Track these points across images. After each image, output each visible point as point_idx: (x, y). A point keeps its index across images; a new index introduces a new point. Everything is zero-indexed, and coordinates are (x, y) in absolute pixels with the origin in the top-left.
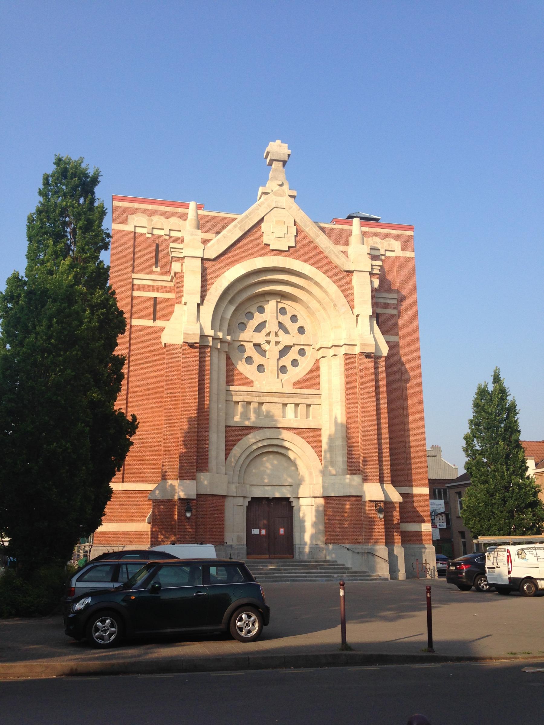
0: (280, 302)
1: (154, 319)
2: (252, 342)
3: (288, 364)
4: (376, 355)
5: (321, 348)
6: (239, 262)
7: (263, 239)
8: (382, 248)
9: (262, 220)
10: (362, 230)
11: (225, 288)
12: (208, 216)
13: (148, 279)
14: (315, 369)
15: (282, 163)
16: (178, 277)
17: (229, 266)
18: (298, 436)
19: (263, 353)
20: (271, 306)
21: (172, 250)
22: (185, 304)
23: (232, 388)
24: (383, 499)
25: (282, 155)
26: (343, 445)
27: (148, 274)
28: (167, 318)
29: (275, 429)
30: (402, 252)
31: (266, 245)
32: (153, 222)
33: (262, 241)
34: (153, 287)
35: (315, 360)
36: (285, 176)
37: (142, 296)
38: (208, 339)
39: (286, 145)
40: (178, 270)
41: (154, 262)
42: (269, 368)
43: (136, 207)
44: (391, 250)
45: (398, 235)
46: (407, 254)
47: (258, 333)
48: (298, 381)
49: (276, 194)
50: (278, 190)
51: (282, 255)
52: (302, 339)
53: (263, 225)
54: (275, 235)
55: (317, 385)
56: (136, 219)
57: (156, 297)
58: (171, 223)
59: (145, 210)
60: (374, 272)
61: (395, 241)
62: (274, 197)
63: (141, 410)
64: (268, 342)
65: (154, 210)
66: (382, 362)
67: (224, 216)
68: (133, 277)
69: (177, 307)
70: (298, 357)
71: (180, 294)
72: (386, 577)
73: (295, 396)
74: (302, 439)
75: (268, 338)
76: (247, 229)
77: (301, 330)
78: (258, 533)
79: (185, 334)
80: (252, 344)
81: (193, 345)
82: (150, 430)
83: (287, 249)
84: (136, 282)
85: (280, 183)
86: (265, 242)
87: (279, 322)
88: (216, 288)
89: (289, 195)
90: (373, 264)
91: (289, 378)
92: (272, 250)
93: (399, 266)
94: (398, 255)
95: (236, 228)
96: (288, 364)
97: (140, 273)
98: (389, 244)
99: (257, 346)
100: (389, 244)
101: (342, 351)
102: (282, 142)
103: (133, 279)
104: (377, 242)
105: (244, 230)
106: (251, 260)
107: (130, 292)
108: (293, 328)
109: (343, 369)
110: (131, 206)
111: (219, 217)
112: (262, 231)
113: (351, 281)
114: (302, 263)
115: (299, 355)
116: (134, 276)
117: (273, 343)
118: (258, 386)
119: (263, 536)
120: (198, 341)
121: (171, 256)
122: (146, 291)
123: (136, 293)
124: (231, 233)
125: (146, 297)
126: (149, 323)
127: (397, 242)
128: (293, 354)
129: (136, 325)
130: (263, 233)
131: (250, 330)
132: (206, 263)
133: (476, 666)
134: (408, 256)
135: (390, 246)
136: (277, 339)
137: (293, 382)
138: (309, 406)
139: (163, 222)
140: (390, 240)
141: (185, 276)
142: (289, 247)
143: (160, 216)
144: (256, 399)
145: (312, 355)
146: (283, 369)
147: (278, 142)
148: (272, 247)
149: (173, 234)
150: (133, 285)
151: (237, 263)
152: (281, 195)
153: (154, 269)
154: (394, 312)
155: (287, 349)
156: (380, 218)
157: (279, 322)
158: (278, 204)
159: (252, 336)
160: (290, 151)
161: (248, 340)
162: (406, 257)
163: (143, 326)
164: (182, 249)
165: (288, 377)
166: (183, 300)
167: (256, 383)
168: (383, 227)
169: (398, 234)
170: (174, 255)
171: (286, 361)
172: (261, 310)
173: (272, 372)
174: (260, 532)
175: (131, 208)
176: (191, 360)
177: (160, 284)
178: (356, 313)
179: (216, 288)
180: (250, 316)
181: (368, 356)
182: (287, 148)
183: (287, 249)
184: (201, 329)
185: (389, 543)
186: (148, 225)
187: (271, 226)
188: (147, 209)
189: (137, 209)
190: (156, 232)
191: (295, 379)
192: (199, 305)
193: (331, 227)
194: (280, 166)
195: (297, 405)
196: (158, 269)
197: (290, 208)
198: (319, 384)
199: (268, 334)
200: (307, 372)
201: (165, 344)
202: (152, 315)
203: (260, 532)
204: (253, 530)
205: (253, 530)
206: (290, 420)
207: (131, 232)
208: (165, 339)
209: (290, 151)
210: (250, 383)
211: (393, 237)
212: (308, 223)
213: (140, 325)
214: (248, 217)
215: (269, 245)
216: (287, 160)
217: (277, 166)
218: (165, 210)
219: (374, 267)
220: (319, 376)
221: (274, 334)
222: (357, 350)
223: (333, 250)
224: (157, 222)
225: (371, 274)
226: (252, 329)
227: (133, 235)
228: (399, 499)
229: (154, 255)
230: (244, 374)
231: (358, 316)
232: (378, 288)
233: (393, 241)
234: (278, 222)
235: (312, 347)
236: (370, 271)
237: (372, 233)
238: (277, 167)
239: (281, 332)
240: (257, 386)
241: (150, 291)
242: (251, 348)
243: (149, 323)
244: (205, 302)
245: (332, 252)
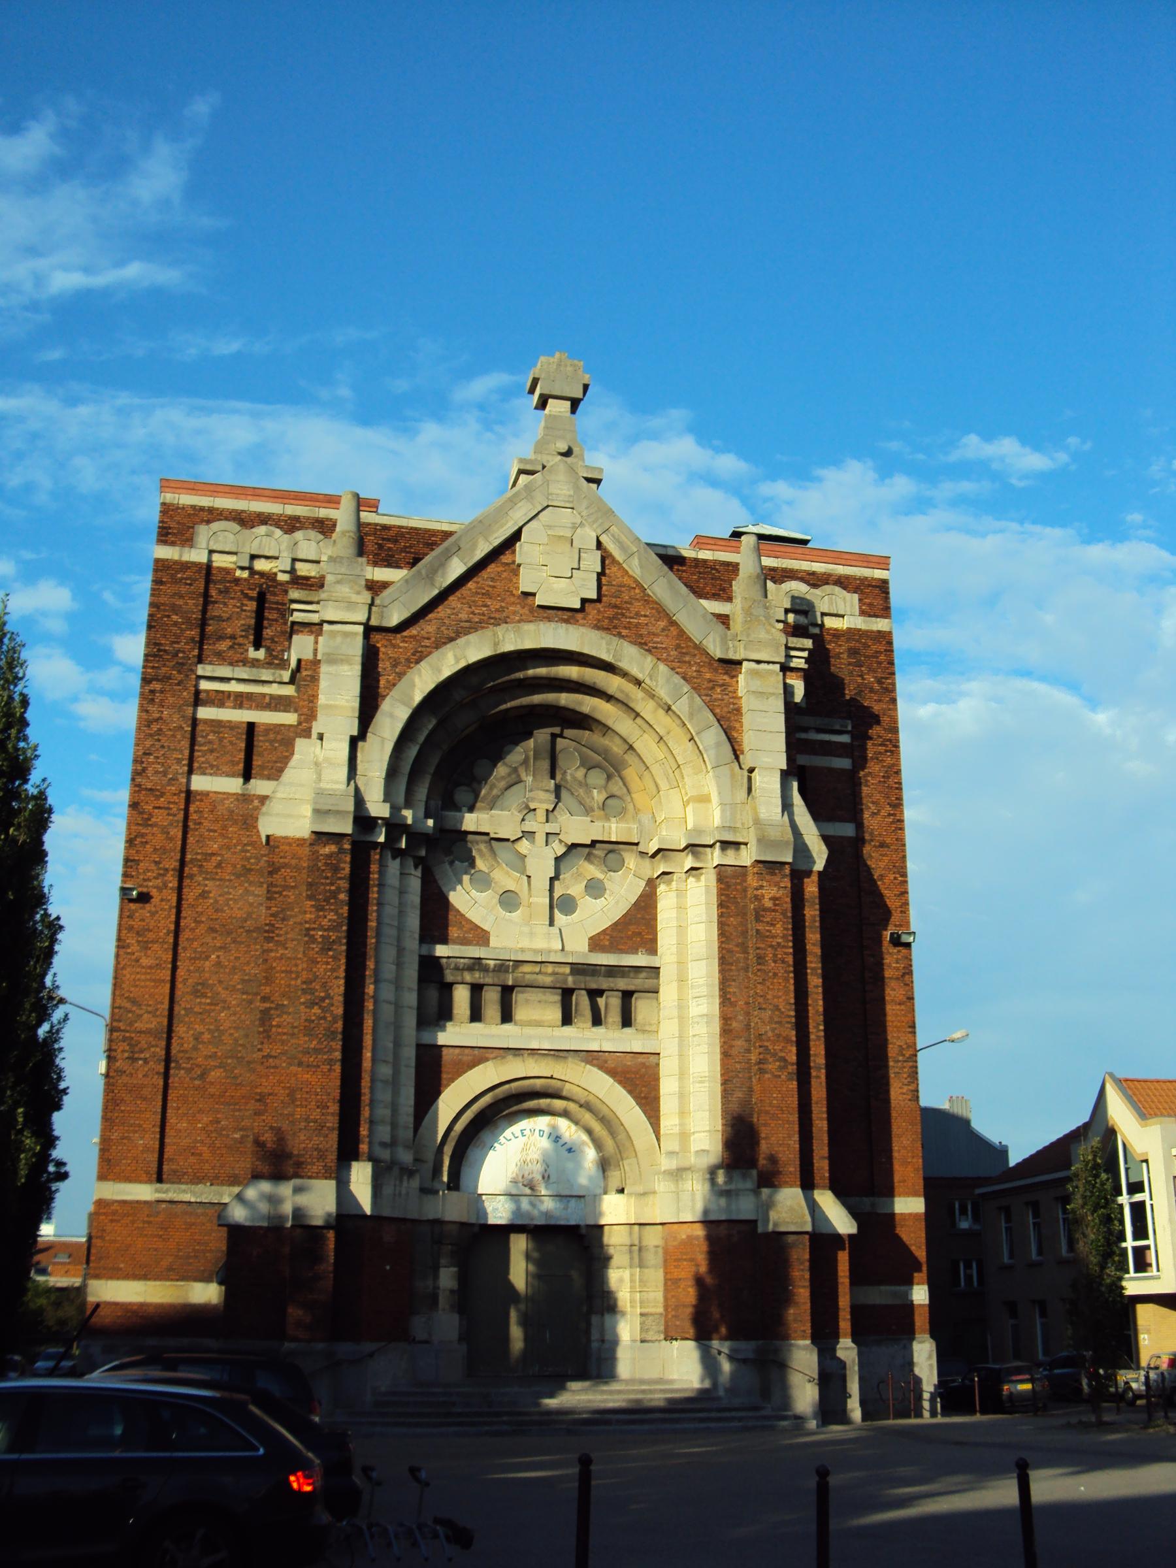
0: (561, 736)
4: (796, 867)
5: (659, 851)
9: (516, 536)
10: (763, 563)
14: (645, 908)
15: (568, 404)
22: (321, 737)
23: (441, 950)
24: (809, 1228)
28: (275, 773)
33: (517, 588)
40: (308, 655)
60: (792, 665)
66: (811, 888)
69: (300, 744)
71: (309, 715)
72: (549, 737)
83: (578, 605)
84: (204, 685)
85: (563, 447)
86: (525, 586)
101: (716, 857)
116: (201, 670)
117: (540, 838)
121: (291, 619)
123: (204, 713)
130: (519, 565)
132: (378, 639)
133: (499, 684)
142: (584, 601)
146: (567, 905)
148: (539, 600)
149: (303, 569)
150: (197, 692)
153: (252, 653)
154: (844, 763)
166: (317, 728)
170: (297, 617)
178: (746, 767)
183: (578, 605)
184: (359, 801)
185: (824, 1338)
190: (260, 565)
192: (354, 742)
196: (261, 654)
201: (268, 837)
208: (268, 826)
215: (534, 595)
216: (580, 396)
219: (793, 653)
225: (785, 668)
231: (751, 770)
232: (804, 705)
243: (232, 785)
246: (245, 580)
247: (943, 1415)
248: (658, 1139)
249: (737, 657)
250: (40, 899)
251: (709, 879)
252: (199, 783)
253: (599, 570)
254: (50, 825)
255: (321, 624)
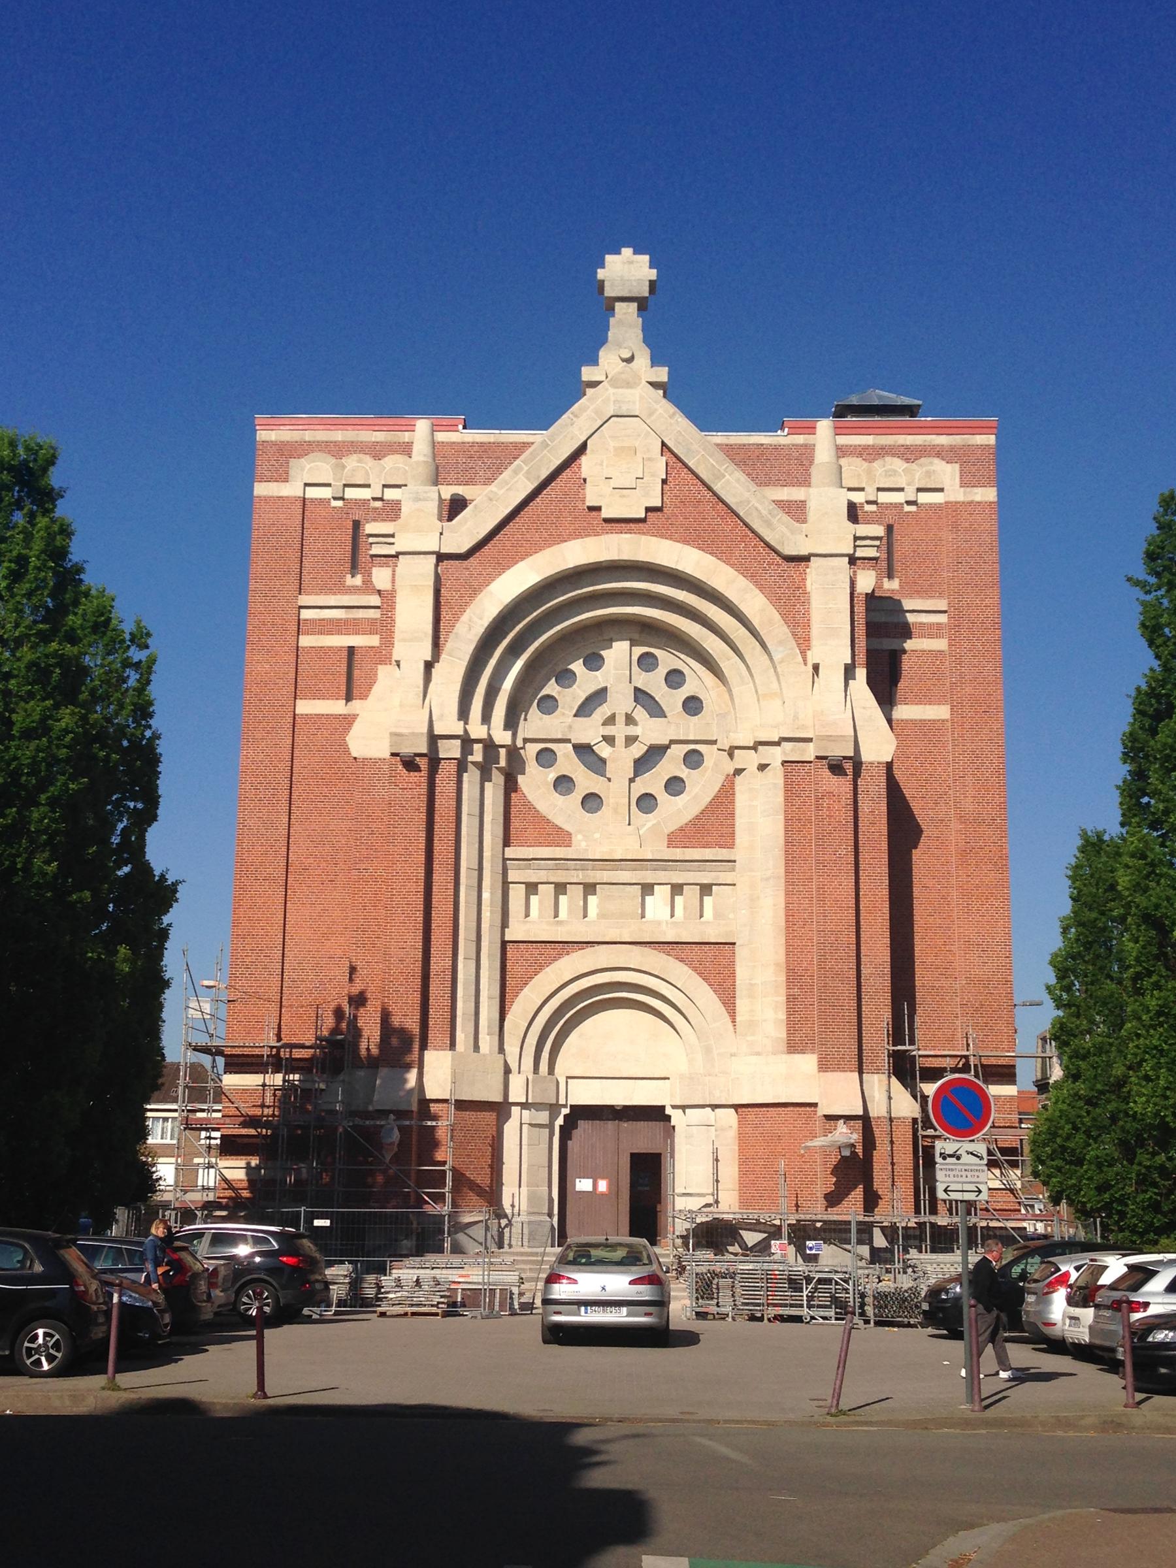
1: (349, 698)
2: (568, 741)
3: (658, 789)
6: (527, 555)
7: (584, 494)
8: (908, 485)
9: (582, 449)
11: (491, 619)
12: (473, 444)
13: (334, 605)
14: (724, 800)
16: (388, 598)
17: (503, 565)
18: (677, 961)
19: (598, 765)
20: (618, 653)
21: (371, 540)
25: (634, 284)
26: (775, 981)
27: (335, 594)
28: (364, 697)
29: (620, 945)
30: (962, 489)
31: (591, 509)
32: (346, 470)
33: (584, 501)
34: (346, 621)
35: (724, 777)
36: (641, 336)
37: (320, 645)
38: (906, 617)
39: (646, 258)
41: (348, 565)
42: (612, 801)
43: (307, 439)
44: (933, 486)
45: (952, 448)
46: (976, 493)
47: (585, 719)
48: (681, 829)
49: (616, 383)
50: (622, 373)
51: (630, 532)
52: (692, 728)
53: (584, 460)
54: (613, 483)
55: (727, 839)
56: (308, 467)
57: (354, 647)
58: (387, 468)
59: (327, 443)
61: (944, 463)
62: (611, 391)
63: (319, 908)
64: (609, 740)
65: (348, 442)
67: (511, 441)
68: (300, 603)
69: (383, 671)
70: (683, 772)
73: (669, 865)
74: (686, 968)
75: (609, 730)
76: (544, 474)
77: (693, 705)
78: (590, 1188)
79: (394, 735)
80: (570, 746)
81: (411, 759)
82: (339, 953)
84: (306, 614)
85: (627, 355)
87: (637, 689)
88: (470, 621)
89: (648, 382)
90: (857, 535)
91: (659, 823)
92: (606, 520)
93: (955, 527)
94: (952, 499)
95: (517, 474)
96: (658, 789)
97: (317, 594)
98: (928, 474)
99: (583, 750)
100: (928, 474)
102: (635, 253)
103: (301, 607)
104: (895, 471)
105: (539, 477)
106: (555, 548)
107: (294, 638)
108: (672, 700)
109: (780, 799)
110: (298, 439)
111: (498, 445)
112: (583, 476)
113: (804, 580)
114: (679, 545)
115: (683, 767)
116: (304, 600)
118: (584, 844)
119: (602, 1194)
120: (425, 751)
122: (330, 633)
123: (306, 641)
124: (507, 487)
125: (330, 648)
126: (337, 707)
127: (949, 465)
128: (673, 764)
129: (307, 715)
131: (566, 712)
134: (978, 498)
135: (930, 477)
136: (632, 731)
137: (667, 831)
138: (706, 889)
139: (368, 468)
140: (931, 463)
141: (398, 599)
143: (361, 456)
144: (578, 876)
145: (716, 764)
147: (627, 252)
148: (605, 513)
151: (523, 559)
152: (628, 385)
153: (350, 581)
155: (655, 753)
156: (919, 402)
157: (637, 689)
158: (620, 407)
159: (570, 727)
160: (655, 271)
161: (560, 736)
162: (972, 502)
163: (323, 715)
164: (393, 536)
165: (655, 822)
167: (577, 838)
168: (910, 431)
169: (954, 443)
170: (376, 550)
171: (652, 782)
172: (594, 662)
173: (616, 811)
174: (595, 1185)
175: (297, 442)
176: (408, 794)
177: (361, 614)
179: (470, 621)
180: (566, 678)
181: (836, 768)
182: (648, 264)
186: (334, 479)
187: (602, 462)
188: (331, 442)
189: (310, 443)
190: (351, 493)
191: (673, 826)
192: (429, 666)
193: (776, 443)
194: (630, 310)
195: (677, 889)
197: (650, 415)
198: (733, 834)
199: (610, 720)
200: (703, 808)
202: (343, 688)
203: (595, 1185)
204: (577, 1180)
205: (577, 1180)
206: (659, 923)
207: (296, 498)
209: (655, 271)
210: (561, 837)
211: (939, 453)
212: (695, 447)
213: (318, 713)
214: (548, 445)
217: (624, 311)
218: (373, 440)
220: (732, 815)
221: (624, 718)
222: (809, 752)
223: (756, 509)
224: (353, 470)
226: (571, 708)
227: (299, 504)
228: (912, 1112)
229: (349, 548)
230: (550, 818)
233: (938, 465)
234: (620, 451)
235: (715, 747)
236: (852, 552)
237: (882, 448)
238: (625, 314)
239: (640, 714)
240: (581, 846)
241: (340, 633)
242: (566, 756)
244: (443, 656)
245: (755, 513)
246: (340, 508)
247: (529, 1247)
248: (734, 1021)
249: (804, 552)
250: (150, 826)
251: (776, 776)
252: (304, 707)
253: (664, 477)
254: (160, 764)
255: (396, 556)
